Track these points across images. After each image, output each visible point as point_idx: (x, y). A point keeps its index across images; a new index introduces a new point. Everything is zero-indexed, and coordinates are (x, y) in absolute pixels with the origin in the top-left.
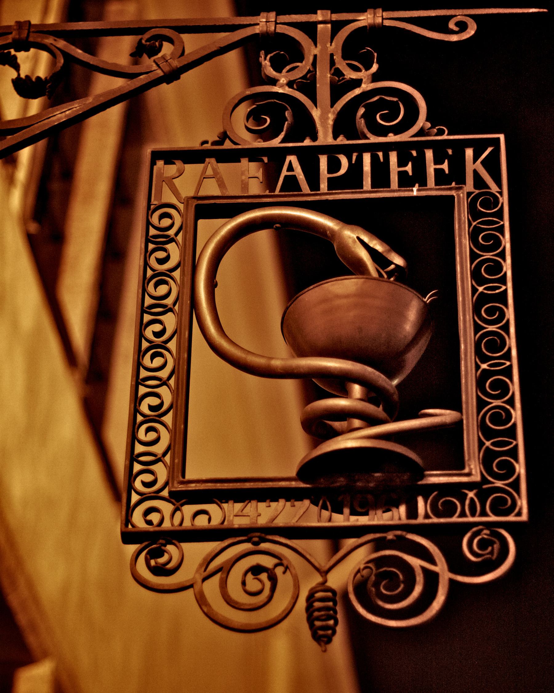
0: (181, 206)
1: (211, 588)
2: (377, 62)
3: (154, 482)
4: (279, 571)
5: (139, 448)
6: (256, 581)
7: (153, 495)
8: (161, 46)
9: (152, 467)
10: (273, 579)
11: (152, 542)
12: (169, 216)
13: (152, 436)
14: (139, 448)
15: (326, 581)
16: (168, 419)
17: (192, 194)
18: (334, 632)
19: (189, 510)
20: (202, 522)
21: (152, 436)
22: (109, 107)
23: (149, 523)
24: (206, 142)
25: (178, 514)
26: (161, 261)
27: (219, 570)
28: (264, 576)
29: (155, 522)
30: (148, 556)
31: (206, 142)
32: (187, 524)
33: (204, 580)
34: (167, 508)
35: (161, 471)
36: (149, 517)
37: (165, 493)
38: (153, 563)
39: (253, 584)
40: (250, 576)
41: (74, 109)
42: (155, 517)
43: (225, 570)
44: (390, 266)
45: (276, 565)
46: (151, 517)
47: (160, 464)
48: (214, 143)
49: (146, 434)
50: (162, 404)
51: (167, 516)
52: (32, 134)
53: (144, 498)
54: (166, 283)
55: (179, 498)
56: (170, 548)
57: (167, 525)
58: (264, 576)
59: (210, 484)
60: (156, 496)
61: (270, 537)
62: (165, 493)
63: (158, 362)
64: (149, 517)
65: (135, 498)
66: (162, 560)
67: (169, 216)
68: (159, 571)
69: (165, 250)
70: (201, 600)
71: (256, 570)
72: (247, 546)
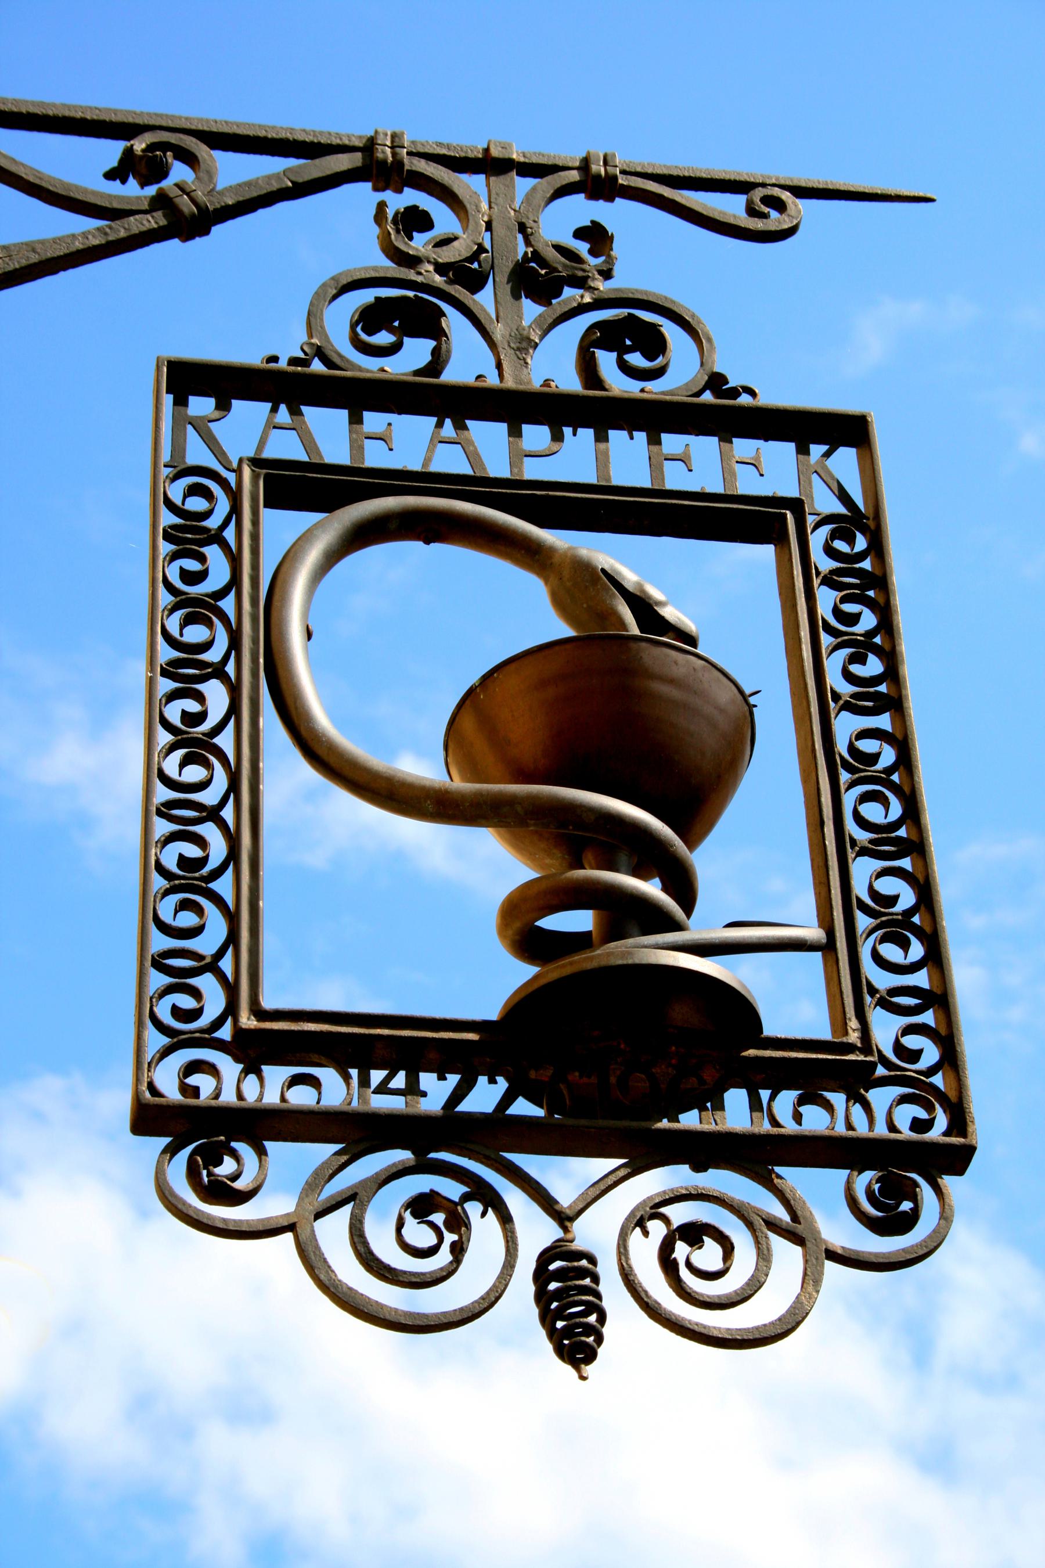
1: (332, 1233)
3: (197, 1014)
4: (473, 1209)
6: (424, 1226)
7: (197, 1035)
9: (193, 981)
10: (458, 1222)
12: (208, 495)
17: (252, 454)
19: (276, 1075)
20: (302, 1097)
22: (701, 215)
24: (274, 359)
27: (350, 1197)
33: (319, 1215)
34: (229, 1068)
36: (193, 1080)
39: (420, 1235)
42: (204, 1083)
45: (466, 1198)
48: (293, 361)
49: (176, 912)
50: (204, 861)
51: (228, 1084)
52: (461, 298)
55: (254, 1051)
57: (228, 1097)
60: (206, 1039)
61: (472, 1147)
62: (225, 1033)
64: (193, 1080)
67: (208, 495)
70: (312, 1260)
72: (402, 1156)
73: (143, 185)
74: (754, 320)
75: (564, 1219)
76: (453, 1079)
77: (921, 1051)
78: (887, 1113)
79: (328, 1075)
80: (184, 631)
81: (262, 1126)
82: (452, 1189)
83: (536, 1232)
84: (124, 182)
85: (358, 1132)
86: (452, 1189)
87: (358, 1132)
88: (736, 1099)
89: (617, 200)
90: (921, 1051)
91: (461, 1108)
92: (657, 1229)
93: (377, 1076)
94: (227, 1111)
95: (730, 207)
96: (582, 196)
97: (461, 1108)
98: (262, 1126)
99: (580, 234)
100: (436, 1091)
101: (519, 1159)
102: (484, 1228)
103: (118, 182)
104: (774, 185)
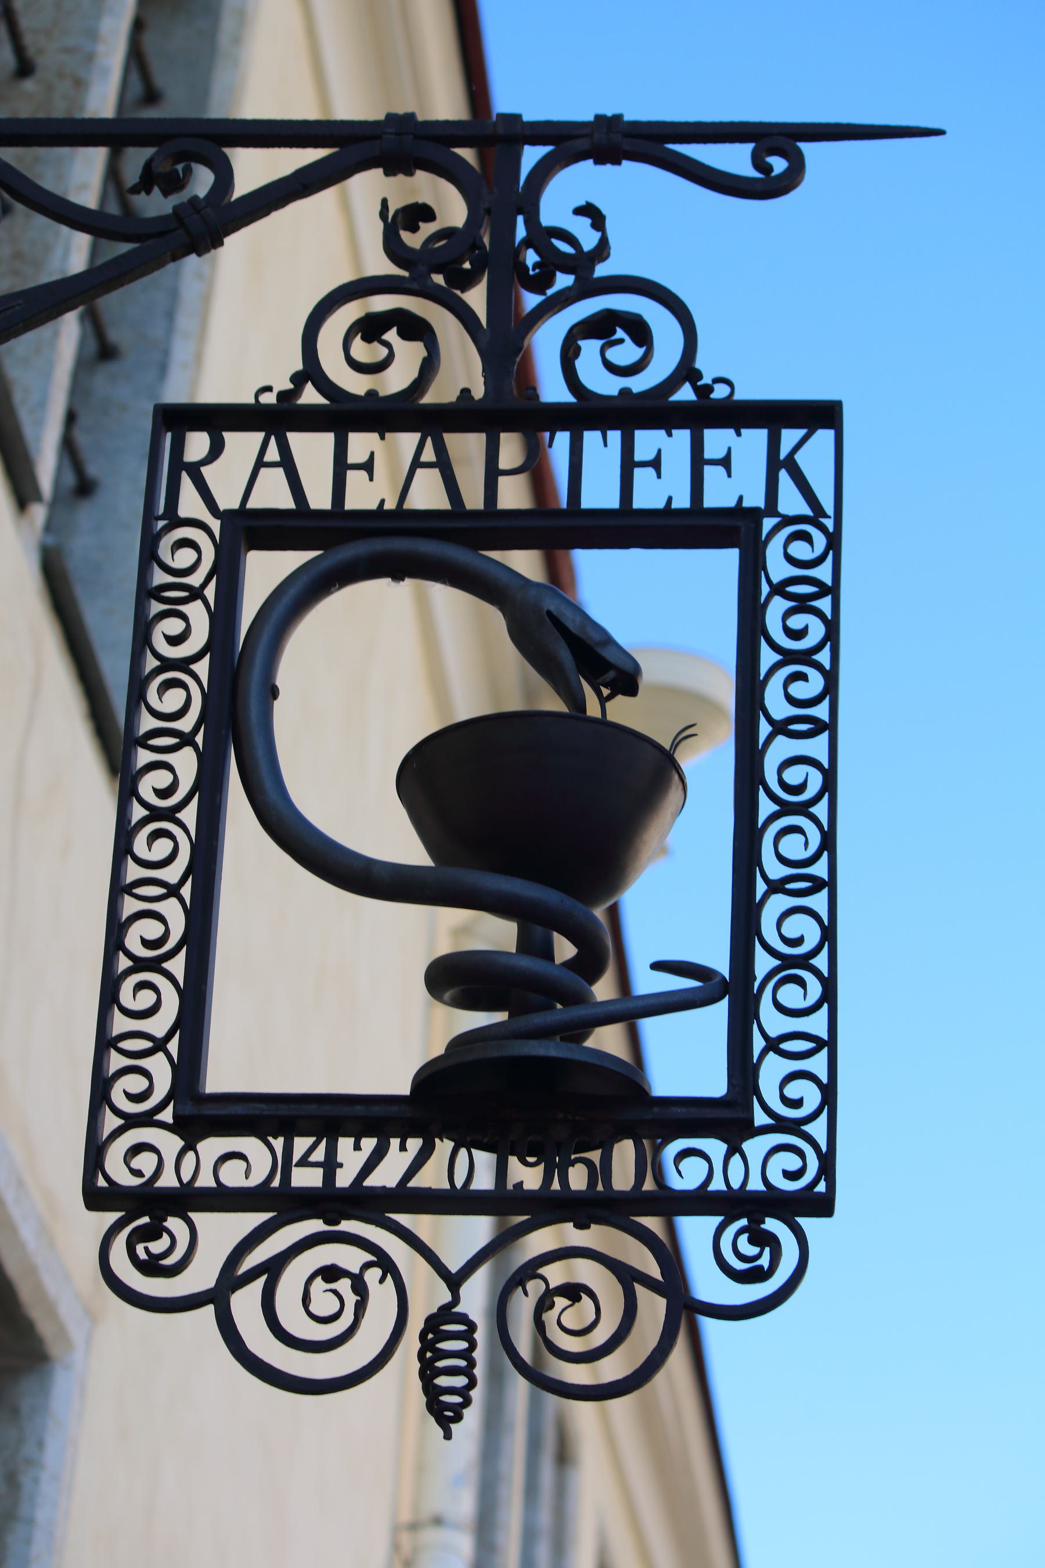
0: (215, 525)
2: (338, 1223)
4: (373, 1276)
5: (121, 1024)
8: (188, 171)
10: (360, 1287)
11: (146, 1209)
13: (146, 998)
14: (121, 1024)
15: (456, 1300)
16: (177, 966)
17: (236, 505)
18: (467, 1402)
21: (146, 998)
23: (138, 1173)
25: (190, 1156)
26: (174, 641)
28: (344, 1285)
29: (148, 1173)
30: (134, 1239)
31: (268, 389)
32: (206, 1180)
34: (170, 1143)
35: (160, 1068)
37: (167, 1116)
38: (140, 1249)
39: (323, 1303)
40: (319, 1284)
41: (17, 308)
42: (146, 1162)
43: (274, 1268)
44: (607, 672)
45: (367, 1266)
46: (136, 1163)
47: (160, 1055)
50: (167, 932)
51: (164, 1158)
53: (132, 1121)
54: (183, 685)
56: (173, 1223)
58: (344, 1285)
59: (263, 1106)
60: (146, 1120)
63: (162, 848)
65: (111, 1122)
66: (158, 1246)
68: (151, 1267)
69: (184, 617)
71: (330, 1273)
72: (315, 1226)
73: (166, 193)
74: (741, 287)
75: (454, 1281)
76: (369, 1144)
77: (807, 627)
78: (763, 1163)
79: (250, 1145)
80: (680, 1168)
81: (188, 1200)
82: (351, 1258)
83: (427, 1294)
84: (148, 192)
85: (280, 1202)
86: (351, 1258)
87: (280, 1202)
88: (625, 1152)
89: (625, 163)
90: (807, 627)
91: (411, 1184)
92: (535, 1288)
93: (301, 1144)
94: (205, 1191)
95: (735, 159)
96: (590, 162)
97: (411, 1184)
98: (188, 1200)
99: (579, 211)
100: (351, 1158)
101: (403, 1219)
102: (382, 1296)
103: (143, 194)
104: (779, 134)
